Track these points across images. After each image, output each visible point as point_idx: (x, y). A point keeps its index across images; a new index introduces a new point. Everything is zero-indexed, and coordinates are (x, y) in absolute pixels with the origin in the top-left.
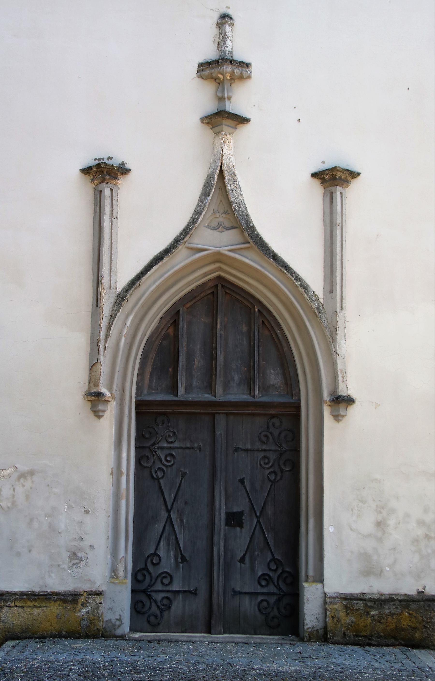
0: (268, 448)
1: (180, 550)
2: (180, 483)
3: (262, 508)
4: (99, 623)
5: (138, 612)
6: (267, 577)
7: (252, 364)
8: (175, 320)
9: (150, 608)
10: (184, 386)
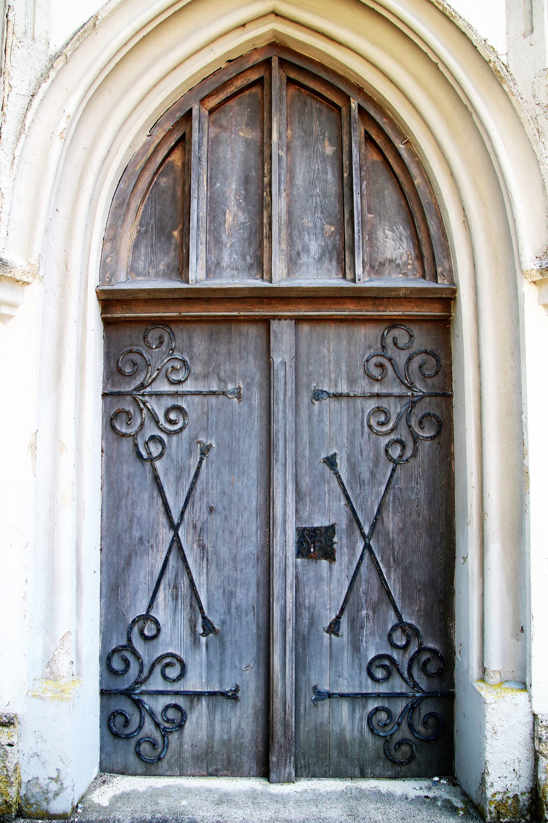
0: (384, 391)
1: (201, 608)
2: (199, 468)
3: (376, 519)
4: (9, 790)
5: (116, 735)
6: (387, 663)
7: (347, 216)
8: (185, 133)
9: (140, 727)
10: (202, 262)
